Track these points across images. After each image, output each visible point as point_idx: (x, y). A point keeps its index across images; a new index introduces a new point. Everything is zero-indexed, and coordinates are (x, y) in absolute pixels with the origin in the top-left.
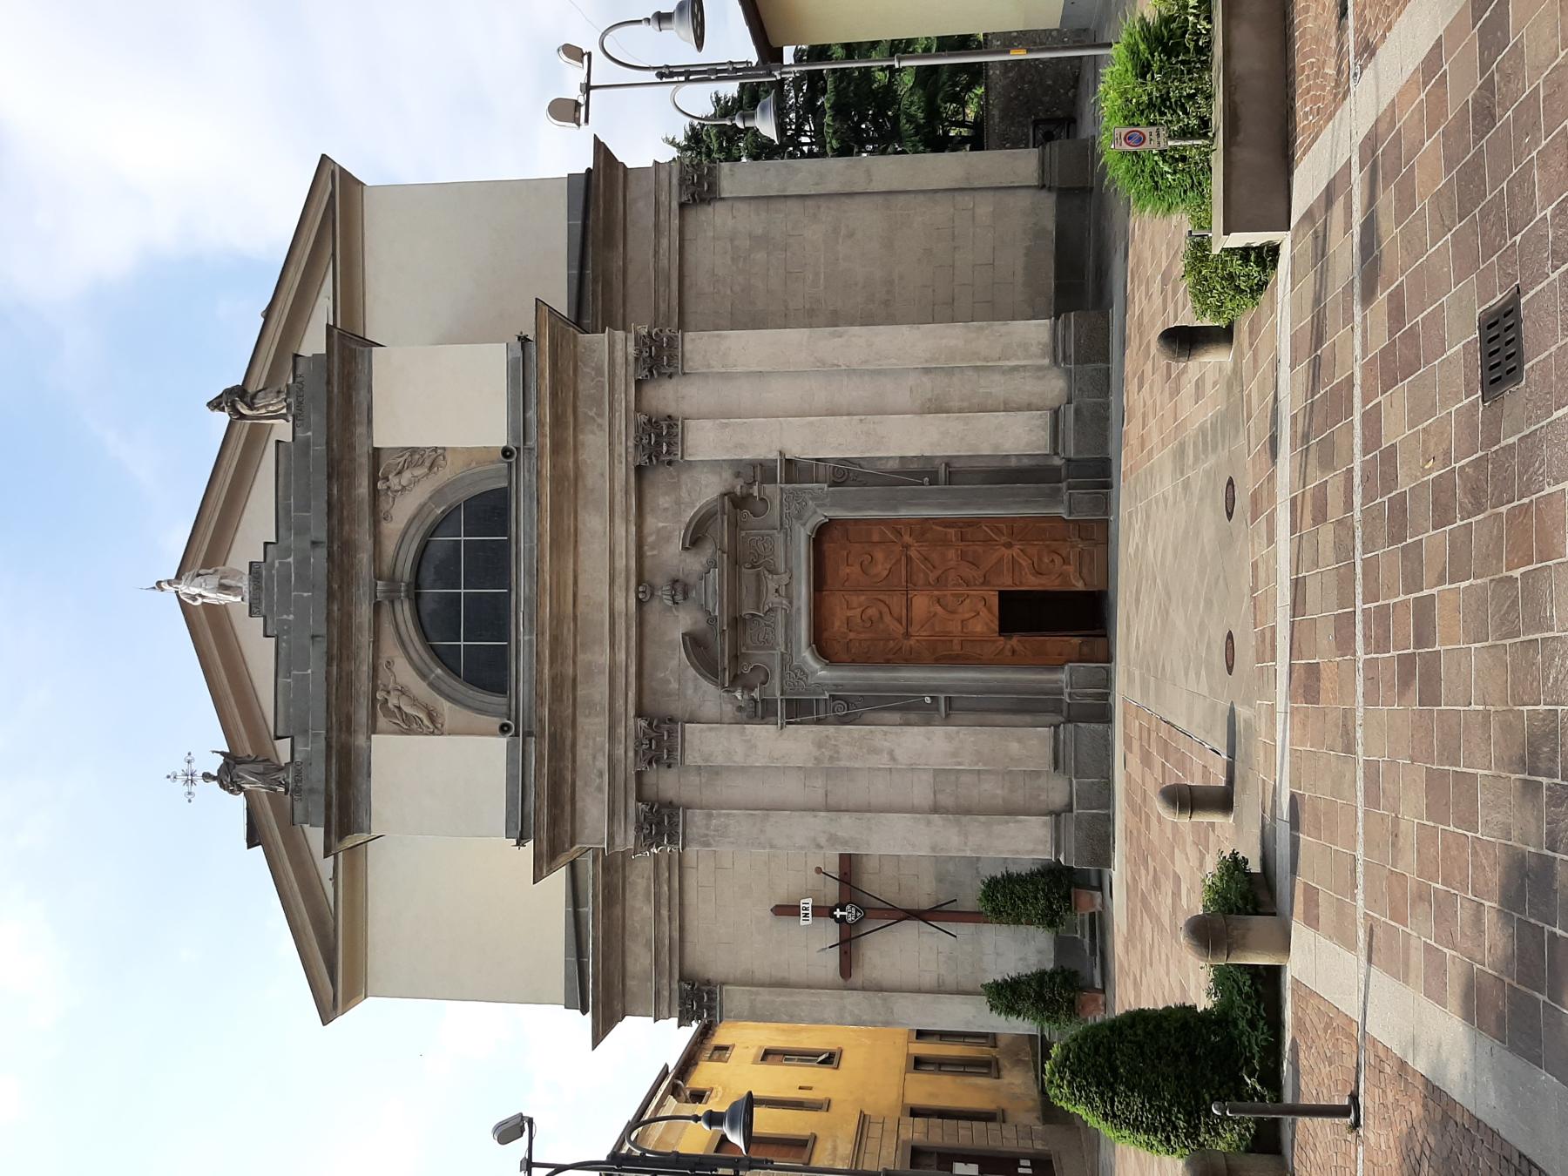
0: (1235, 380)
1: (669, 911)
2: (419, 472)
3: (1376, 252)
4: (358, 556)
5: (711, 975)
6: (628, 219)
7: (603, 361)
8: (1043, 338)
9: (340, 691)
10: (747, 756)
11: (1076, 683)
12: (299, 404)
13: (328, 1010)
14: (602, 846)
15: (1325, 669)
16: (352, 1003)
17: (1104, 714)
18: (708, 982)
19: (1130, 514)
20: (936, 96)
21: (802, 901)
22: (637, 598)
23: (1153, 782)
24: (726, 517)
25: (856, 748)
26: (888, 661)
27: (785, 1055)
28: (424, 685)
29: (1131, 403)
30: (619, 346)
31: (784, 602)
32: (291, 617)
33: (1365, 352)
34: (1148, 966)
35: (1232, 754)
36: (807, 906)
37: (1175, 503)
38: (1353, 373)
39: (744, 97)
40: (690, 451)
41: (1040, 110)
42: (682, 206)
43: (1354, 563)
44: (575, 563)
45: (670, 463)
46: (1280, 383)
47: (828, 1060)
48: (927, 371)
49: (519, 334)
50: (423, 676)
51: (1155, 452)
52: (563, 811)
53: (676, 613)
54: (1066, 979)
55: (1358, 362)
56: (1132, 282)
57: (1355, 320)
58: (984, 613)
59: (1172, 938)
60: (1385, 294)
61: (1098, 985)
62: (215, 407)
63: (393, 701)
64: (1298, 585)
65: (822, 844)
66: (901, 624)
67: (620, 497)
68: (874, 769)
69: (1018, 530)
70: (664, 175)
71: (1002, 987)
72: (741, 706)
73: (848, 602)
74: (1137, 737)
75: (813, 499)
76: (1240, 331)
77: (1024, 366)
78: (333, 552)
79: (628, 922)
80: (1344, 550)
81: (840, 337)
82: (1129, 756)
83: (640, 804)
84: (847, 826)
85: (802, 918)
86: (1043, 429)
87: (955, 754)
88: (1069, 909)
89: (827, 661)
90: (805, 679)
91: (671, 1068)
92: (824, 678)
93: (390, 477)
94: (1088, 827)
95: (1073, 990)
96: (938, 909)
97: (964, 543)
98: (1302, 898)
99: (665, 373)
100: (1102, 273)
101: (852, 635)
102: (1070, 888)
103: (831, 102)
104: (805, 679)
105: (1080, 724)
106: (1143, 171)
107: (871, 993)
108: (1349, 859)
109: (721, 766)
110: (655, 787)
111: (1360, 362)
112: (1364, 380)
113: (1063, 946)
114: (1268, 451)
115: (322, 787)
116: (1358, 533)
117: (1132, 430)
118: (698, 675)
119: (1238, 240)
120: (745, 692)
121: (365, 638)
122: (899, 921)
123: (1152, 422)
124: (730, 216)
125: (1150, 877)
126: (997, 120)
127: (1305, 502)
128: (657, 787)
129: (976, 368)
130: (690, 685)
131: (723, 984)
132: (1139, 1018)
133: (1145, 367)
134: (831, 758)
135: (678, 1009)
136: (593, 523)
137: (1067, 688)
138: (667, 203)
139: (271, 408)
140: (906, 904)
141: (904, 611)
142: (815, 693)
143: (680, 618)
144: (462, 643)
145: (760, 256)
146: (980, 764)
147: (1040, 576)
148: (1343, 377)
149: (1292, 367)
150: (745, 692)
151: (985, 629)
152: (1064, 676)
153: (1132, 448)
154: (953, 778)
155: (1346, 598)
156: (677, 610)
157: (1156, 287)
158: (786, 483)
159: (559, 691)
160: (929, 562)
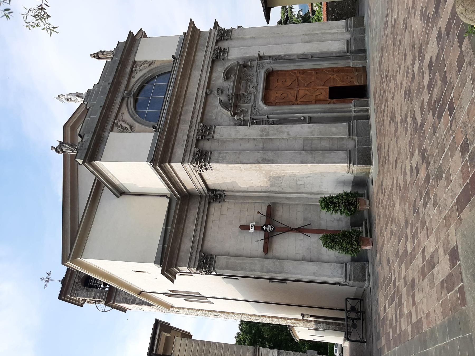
1: (201, 227)
5: (212, 253)
10: (236, 135)
11: (356, 105)
21: (251, 223)
22: (206, 92)
24: (238, 67)
36: (253, 225)
44: (188, 83)
45: (223, 59)
48: (306, 35)
50: (132, 117)
65: (260, 161)
87: (312, 132)
105: (358, 120)
107: (275, 260)
121: (117, 107)
135: (198, 263)
136: (196, 74)
139: (108, 55)
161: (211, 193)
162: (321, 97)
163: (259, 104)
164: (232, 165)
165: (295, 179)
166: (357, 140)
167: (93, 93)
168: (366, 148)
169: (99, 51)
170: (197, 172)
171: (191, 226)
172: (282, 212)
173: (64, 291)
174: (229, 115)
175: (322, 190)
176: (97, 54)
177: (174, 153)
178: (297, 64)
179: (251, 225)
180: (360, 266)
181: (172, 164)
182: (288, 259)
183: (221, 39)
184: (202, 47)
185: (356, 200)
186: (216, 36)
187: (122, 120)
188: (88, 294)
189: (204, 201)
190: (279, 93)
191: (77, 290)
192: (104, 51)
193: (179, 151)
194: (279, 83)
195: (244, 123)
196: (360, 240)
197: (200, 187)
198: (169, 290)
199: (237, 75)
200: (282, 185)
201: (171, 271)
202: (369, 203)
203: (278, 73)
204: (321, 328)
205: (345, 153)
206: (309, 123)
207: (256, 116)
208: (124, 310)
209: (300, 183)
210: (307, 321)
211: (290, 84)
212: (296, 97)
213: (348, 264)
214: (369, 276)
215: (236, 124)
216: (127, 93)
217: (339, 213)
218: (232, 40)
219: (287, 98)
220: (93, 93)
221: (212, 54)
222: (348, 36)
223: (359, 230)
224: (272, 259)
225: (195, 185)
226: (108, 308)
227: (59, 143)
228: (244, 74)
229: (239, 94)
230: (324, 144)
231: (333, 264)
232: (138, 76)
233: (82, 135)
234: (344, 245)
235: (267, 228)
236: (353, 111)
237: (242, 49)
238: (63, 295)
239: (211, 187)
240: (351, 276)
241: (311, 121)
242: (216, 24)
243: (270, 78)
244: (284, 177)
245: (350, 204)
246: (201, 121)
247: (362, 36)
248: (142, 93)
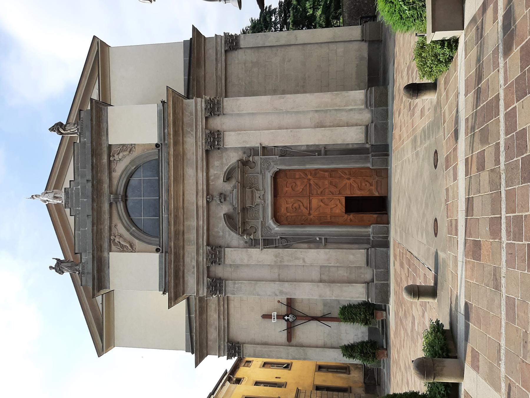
0: (438, 106)
1: (224, 316)
2: (125, 153)
3: (513, 27)
4: (104, 185)
6: (206, 57)
7: (193, 110)
8: (362, 98)
9: (97, 235)
10: (249, 260)
12: (82, 128)
13: (100, 352)
14: (194, 295)
15: (483, 244)
16: (110, 348)
17: (386, 244)
18: (238, 343)
19: (396, 166)
20: (329, 16)
22: (207, 201)
23: (404, 275)
24: (239, 169)
25: (290, 258)
26: (302, 224)
27: (272, 364)
28: (128, 233)
29: (396, 122)
30: (199, 104)
31: (262, 201)
32: (80, 208)
33: (506, 80)
34: (402, 347)
35: (436, 272)
36: (274, 315)
37: (412, 162)
38: (499, 93)
39: (261, 19)
40: (226, 144)
41: (363, 13)
42: (226, 51)
43: (501, 192)
44: (183, 187)
45: (219, 149)
46: (459, 104)
47: (287, 367)
49: (162, 100)
50: (128, 230)
51: (405, 140)
52: (180, 280)
53: (221, 206)
54: (372, 345)
55: (502, 88)
56: (396, 73)
57: (500, 66)
58: (339, 205)
59: (412, 341)
60: (519, 48)
61: (385, 347)
62: (52, 130)
63: (117, 240)
64: (469, 201)
65: (277, 294)
66: (307, 210)
67: (200, 162)
68: (298, 265)
69: (353, 173)
70: (219, 40)
71: (348, 348)
72: (246, 241)
73: (287, 201)
74: (398, 255)
75: (273, 162)
76: (440, 84)
77: (355, 109)
78: (94, 184)
79: (209, 321)
80: (495, 185)
81: (283, 98)
82: (395, 262)
83: (208, 279)
84: (287, 287)
85: (273, 320)
86: (362, 133)
87: (328, 260)
88: (373, 318)
89: (279, 224)
90: (270, 231)
91: (228, 371)
92: (278, 231)
93: (115, 155)
94: (380, 288)
95: (375, 350)
96: (324, 316)
97: (331, 178)
98: (470, 354)
99: (217, 114)
100: (385, 72)
101: (288, 214)
102: (374, 310)
103: (292, 20)
104: (270, 231)
105: (376, 248)
106: (395, 11)
107: (299, 348)
108: (497, 345)
109: (239, 264)
110: (214, 272)
111: (503, 87)
112: (506, 96)
113: (371, 331)
114: (454, 136)
115: (91, 271)
116: (503, 176)
117: (396, 132)
118: (229, 230)
119: (440, 35)
120: (248, 236)
121: (106, 216)
122: (309, 321)
123: (404, 129)
124: (244, 55)
125: (403, 312)
126: (347, 18)
127: (473, 160)
128: (215, 272)
129: (336, 110)
130: (227, 233)
131: (244, 343)
132: (395, 395)
133: (401, 107)
134: (281, 261)
136: (190, 172)
137: (371, 234)
138: (220, 51)
140: (313, 314)
141: (308, 205)
142: (274, 237)
143: (223, 207)
144: (142, 218)
145: (255, 70)
146: (338, 264)
147: (361, 191)
148: (493, 96)
149: (466, 95)
150: (248, 236)
151: (340, 212)
152: (370, 230)
153: (396, 140)
155: (496, 208)
156: (222, 205)
157: (405, 73)
158: (262, 156)
159: (177, 236)
160: (318, 186)
166: (376, 274)
168: (384, 283)
171: (214, 315)
177: (186, 282)
179: (273, 315)
214: (384, 363)
227: (55, 261)
235: (289, 318)
237: (240, 134)
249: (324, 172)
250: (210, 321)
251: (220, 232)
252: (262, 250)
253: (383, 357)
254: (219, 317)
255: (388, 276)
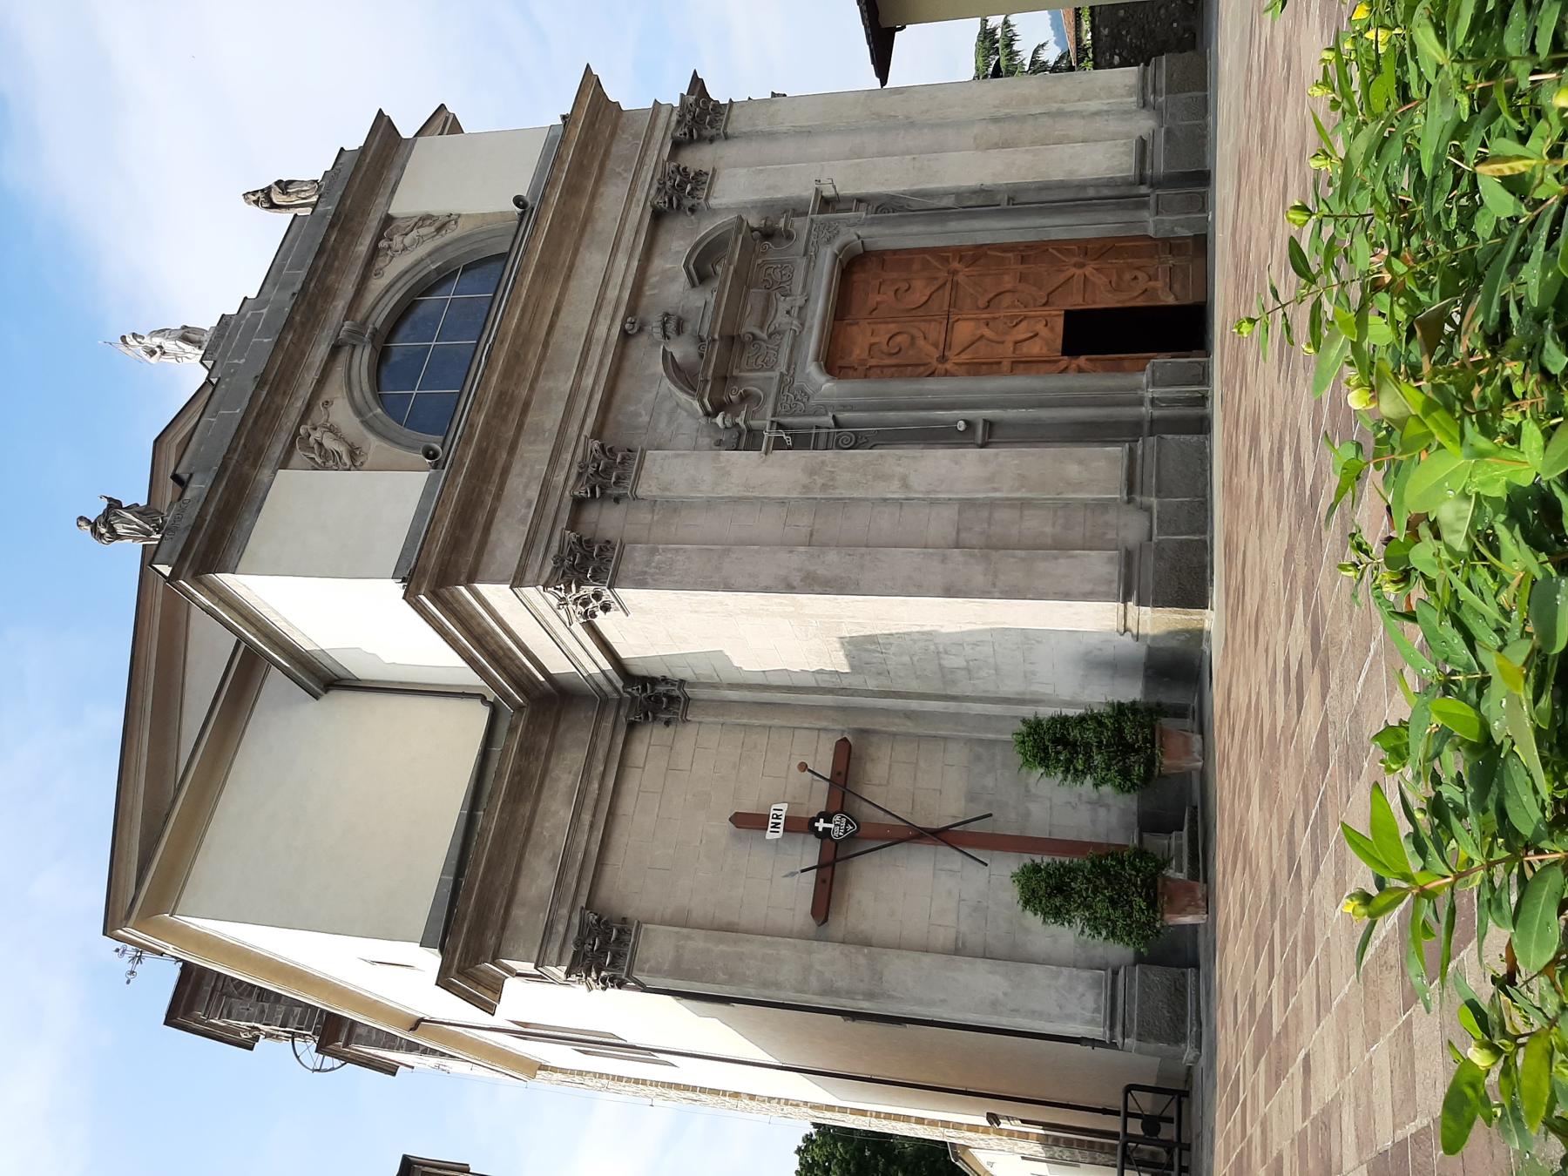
1: (594, 816)
17: (1202, 426)
24: (740, 237)
36: (779, 813)
45: (692, 210)
48: (995, 120)
50: (358, 412)
65: (795, 584)
79: (536, 829)
87: (990, 479)
107: (852, 949)
110: (593, 525)
121: (310, 378)
128: (597, 526)
136: (592, 262)
154: (985, 514)
161: (635, 691)
162: (1035, 349)
163: (807, 371)
164: (696, 595)
165: (932, 647)
166: (1158, 512)
167: (237, 326)
168: (1192, 541)
169: (271, 182)
170: (574, 619)
172: (890, 765)
173: (185, 996)
174: (698, 411)
175: (1035, 688)
176: (267, 192)
177: (489, 547)
178: (953, 225)
179: (772, 812)
180: (1168, 983)
181: (482, 588)
182: (899, 946)
183: (692, 136)
184: (623, 167)
185: (1153, 734)
186: (673, 124)
187: (323, 426)
188: (262, 1011)
189: (611, 719)
190: (884, 332)
191: (230, 996)
192: (291, 182)
193: (508, 541)
194: (887, 296)
195: (748, 440)
196: (1160, 890)
197: (594, 667)
198: (512, 1022)
199: (732, 268)
200: (889, 667)
201: (479, 973)
202: (1204, 750)
203: (884, 260)
204: (1064, 1157)
205: (1110, 560)
206: (982, 446)
207: (792, 415)
208: (390, 1069)
209: (951, 662)
210: (1011, 1134)
211: (925, 298)
212: (942, 346)
213: (1122, 972)
215: (719, 444)
216: (348, 331)
217: (1089, 781)
218: (729, 142)
219: (911, 352)
220: (237, 326)
221: (653, 192)
222: (1145, 124)
223: (1166, 842)
224: (843, 942)
225: (576, 663)
226: (329, 1062)
227: (106, 502)
228: (760, 261)
229: (739, 336)
230: (1036, 524)
231: (1065, 971)
232: (394, 268)
233: (185, 477)
234: (1102, 909)
235: (832, 826)
236: (1147, 403)
238: (181, 1009)
239: (637, 670)
240: (1132, 1020)
241: (990, 435)
242: (697, 84)
243: (856, 277)
244: (891, 641)
245: (1127, 749)
246: (597, 434)
247: (1197, 122)
248: (405, 329)
249: (1004, 251)
250: (542, 833)
251: (641, 416)
252: (769, 455)
253: (1190, 905)
254: (576, 815)
255: (1206, 510)
